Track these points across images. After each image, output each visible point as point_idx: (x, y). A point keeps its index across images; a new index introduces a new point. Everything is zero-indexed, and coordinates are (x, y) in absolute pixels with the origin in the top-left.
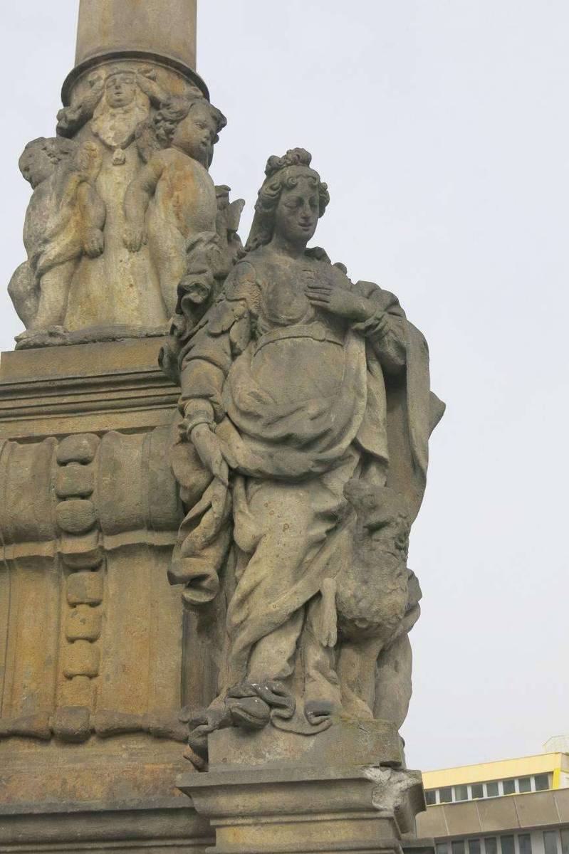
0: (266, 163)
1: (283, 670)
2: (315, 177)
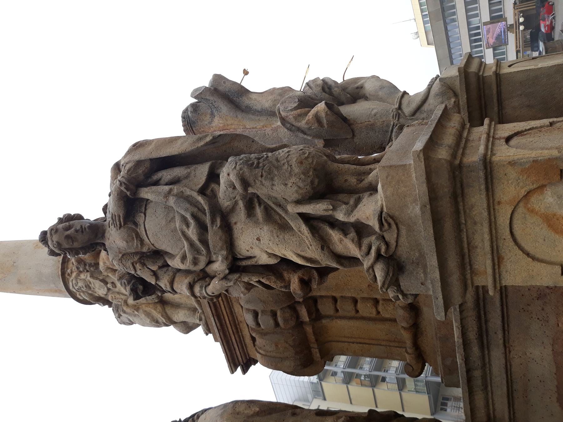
0: (181, 119)
1: (353, 241)
2: (52, 229)
